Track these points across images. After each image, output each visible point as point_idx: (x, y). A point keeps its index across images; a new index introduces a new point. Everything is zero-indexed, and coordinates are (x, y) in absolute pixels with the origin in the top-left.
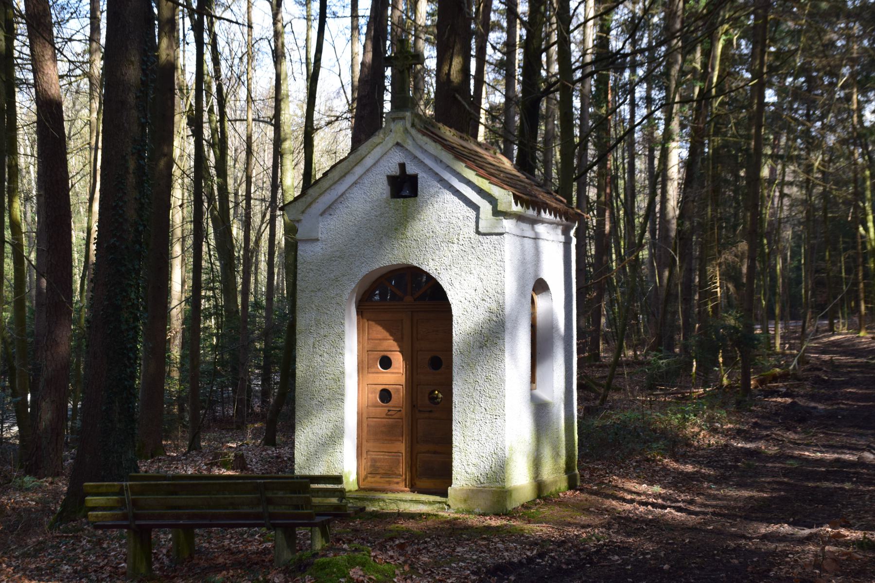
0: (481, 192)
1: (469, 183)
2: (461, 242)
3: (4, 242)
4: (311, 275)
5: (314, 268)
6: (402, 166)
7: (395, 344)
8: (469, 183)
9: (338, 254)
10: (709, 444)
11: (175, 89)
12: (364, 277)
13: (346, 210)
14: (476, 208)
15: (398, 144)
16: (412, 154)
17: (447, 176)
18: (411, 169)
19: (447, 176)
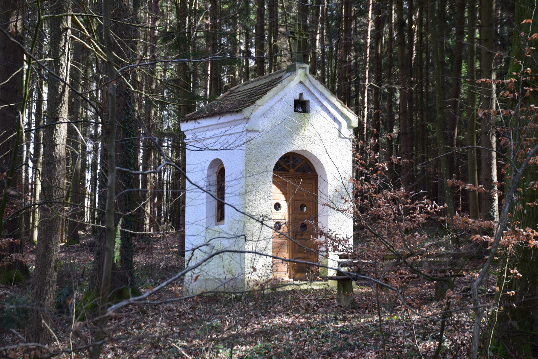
0: (342, 114)
1: (337, 109)
2: (332, 141)
3: (40, 143)
4: (254, 152)
5: (255, 148)
6: (301, 95)
7: (283, 196)
8: (337, 109)
9: (269, 141)
10: (146, 255)
11: (34, 138)
12: (286, 154)
13: (273, 115)
14: (339, 123)
15: (301, 82)
16: (307, 88)
17: (325, 103)
18: (306, 97)
19: (325, 103)
